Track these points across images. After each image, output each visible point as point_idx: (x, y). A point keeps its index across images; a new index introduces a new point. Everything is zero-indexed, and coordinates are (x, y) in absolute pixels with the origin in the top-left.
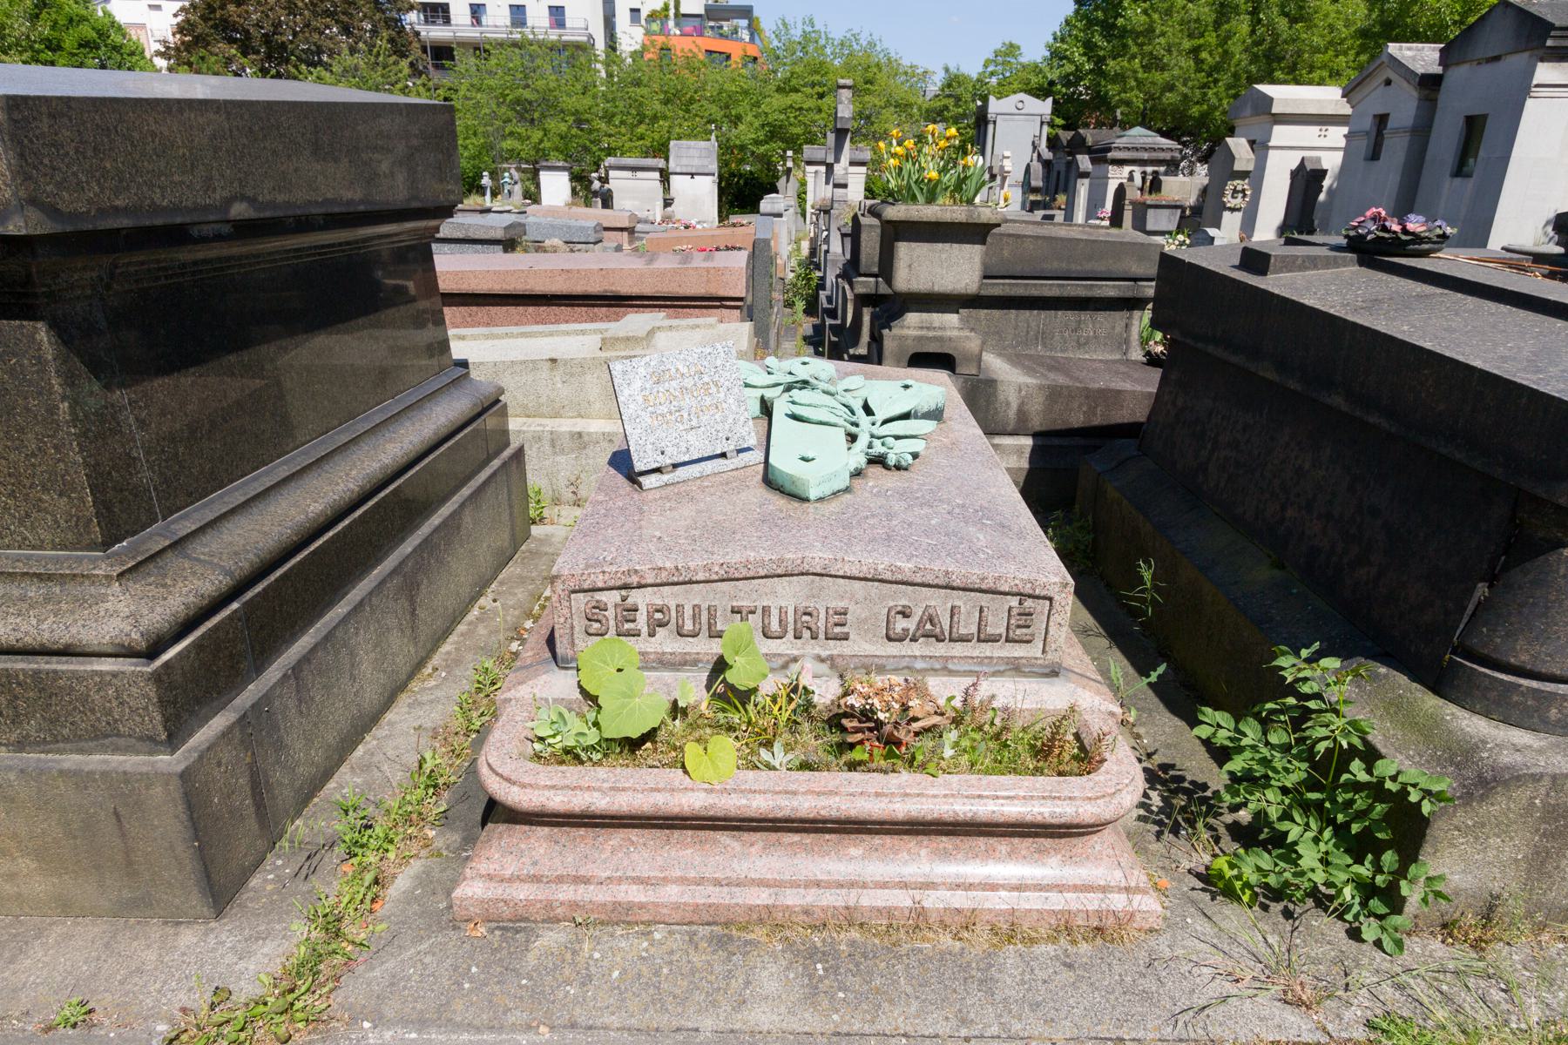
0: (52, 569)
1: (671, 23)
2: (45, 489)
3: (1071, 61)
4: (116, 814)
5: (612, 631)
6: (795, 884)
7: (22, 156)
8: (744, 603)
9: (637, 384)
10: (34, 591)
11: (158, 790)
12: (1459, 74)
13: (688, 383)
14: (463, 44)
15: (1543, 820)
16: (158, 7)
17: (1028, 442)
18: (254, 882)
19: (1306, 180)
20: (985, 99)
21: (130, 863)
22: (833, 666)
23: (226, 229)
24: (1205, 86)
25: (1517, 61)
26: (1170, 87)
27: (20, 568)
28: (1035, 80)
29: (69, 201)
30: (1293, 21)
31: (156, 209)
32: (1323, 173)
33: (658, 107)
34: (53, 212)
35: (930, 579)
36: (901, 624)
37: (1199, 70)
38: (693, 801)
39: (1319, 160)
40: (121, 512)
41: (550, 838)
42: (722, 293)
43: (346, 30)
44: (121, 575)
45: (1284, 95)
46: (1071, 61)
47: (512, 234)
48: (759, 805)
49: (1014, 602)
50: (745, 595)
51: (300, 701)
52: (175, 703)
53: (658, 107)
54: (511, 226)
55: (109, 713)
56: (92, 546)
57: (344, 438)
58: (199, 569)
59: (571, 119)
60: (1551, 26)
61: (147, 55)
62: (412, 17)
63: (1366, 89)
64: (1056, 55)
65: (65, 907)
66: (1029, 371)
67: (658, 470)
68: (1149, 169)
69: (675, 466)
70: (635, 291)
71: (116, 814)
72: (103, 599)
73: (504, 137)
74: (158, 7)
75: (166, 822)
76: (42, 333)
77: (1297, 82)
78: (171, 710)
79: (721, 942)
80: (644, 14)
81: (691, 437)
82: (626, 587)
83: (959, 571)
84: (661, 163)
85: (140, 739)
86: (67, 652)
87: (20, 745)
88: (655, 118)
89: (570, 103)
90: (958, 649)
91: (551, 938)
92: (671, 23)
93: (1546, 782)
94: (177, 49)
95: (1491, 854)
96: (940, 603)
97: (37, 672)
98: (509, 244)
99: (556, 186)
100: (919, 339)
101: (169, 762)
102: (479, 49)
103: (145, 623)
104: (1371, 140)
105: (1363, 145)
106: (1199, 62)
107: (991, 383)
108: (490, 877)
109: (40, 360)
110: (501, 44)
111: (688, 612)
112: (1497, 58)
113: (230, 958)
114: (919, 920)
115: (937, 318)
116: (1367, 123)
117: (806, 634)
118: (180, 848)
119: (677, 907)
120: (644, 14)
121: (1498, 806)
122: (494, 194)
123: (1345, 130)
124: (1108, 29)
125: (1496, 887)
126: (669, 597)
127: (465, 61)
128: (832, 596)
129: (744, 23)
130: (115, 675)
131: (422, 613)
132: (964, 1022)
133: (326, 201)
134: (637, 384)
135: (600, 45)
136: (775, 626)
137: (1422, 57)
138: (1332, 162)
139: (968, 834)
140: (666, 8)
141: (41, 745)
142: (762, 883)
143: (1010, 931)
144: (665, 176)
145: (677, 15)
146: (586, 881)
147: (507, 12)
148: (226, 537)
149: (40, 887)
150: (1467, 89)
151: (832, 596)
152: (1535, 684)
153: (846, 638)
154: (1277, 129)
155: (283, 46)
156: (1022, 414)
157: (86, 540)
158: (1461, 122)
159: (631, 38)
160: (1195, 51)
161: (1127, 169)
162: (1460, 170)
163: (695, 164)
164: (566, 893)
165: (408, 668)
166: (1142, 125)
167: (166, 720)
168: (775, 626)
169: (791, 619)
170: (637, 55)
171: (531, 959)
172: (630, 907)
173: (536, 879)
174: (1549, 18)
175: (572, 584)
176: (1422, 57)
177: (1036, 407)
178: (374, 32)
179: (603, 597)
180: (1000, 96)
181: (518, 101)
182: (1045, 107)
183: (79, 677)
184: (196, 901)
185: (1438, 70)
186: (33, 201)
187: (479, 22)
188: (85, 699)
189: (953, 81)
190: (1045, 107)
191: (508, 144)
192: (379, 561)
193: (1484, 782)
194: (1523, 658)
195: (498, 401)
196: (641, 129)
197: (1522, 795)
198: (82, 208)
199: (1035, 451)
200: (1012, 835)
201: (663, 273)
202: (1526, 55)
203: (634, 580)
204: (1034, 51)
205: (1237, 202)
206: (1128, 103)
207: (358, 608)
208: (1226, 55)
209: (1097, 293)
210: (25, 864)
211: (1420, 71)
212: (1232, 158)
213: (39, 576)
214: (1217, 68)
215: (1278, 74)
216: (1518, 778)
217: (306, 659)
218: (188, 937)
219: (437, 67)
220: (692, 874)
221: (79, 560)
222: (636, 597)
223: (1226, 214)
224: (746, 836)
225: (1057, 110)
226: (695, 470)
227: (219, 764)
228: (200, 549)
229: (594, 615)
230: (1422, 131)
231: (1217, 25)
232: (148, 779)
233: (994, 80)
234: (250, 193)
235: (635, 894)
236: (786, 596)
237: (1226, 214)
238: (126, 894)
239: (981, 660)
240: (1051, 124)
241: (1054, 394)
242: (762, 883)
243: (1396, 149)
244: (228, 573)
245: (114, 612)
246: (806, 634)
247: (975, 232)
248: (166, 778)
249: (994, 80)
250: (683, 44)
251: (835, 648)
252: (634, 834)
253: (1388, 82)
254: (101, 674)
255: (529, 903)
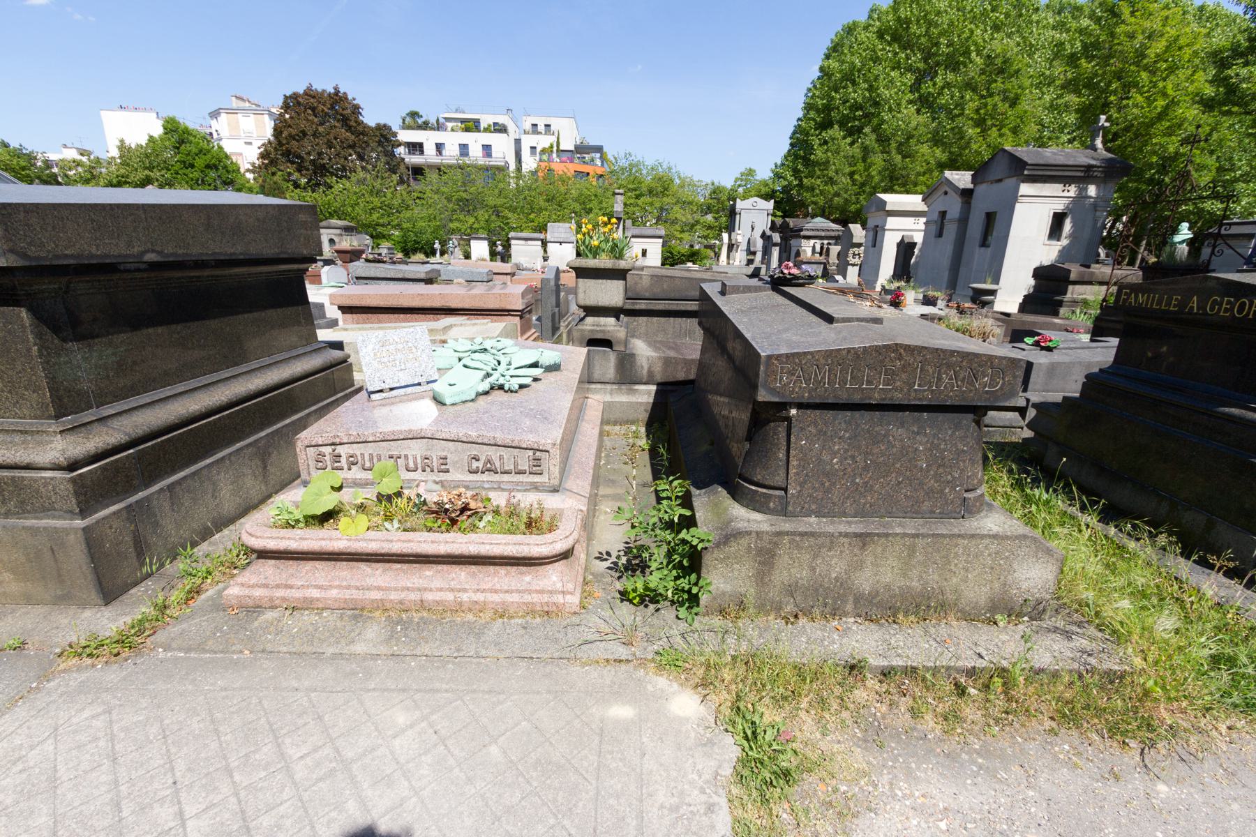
0: (28, 428)
1: (554, 155)
2: (26, 389)
3: (785, 179)
4: (52, 549)
5: (329, 467)
6: (396, 589)
7: (6, 230)
8: (395, 453)
9: (370, 347)
10: (18, 438)
11: (72, 537)
12: (982, 189)
13: (400, 346)
14: (431, 166)
15: (757, 555)
16: (250, 143)
17: (654, 388)
18: (132, 591)
19: (906, 248)
20: (734, 200)
21: (60, 576)
22: (443, 486)
23: (143, 266)
24: (859, 194)
25: (1010, 182)
26: (837, 194)
27: (12, 427)
28: (764, 190)
29: (33, 251)
30: (904, 157)
31: (93, 256)
32: (915, 244)
33: (542, 203)
34: (24, 256)
35: (485, 441)
36: (475, 464)
37: (854, 184)
38: (339, 545)
39: (912, 237)
40: (66, 404)
41: (275, 566)
42: (509, 307)
43: (361, 158)
44: (61, 432)
45: (893, 200)
46: (785, 179)
47: (430, 276)
48: (373, 547)
49: (531, 453)
50: (395, 449)
51: (173, 504)
52: (85, 494)
53: (542, 203)
54: (433, 271)
55: (50, 498)
56: (50, 417)
57: (227, 375)
58: (111, 432)
59: (491, 211)
60: (1026, 163)
61: (242, 170)
62: (401, 151)
63: (935, 196)
64: (778, 176)
65: (29, 600)
66: (656, 349)
67: (381, 391)
68: (826, 242)
69: (391, 389)
70: (460, 306)
71: (52, 549)
72: (51, 442)
73: (451, 221)
74: (250, 143)
75: (77, 555)
76: (24, 313)
77: (908, 192)
78: (82, 498)
79: (355, 617)
80: (538, 150)
81: (401, 374)
82: (333, 444)
83: (500, 437)
84: (542, 236)
85: (66, 512)
86: (28, 467)
87: (7, 515)
88: (541, 210)
89: (491, 201)
90: (506, 478)
91: (270, 615)
92: (554, 155)
93: (754, 535)
94: (260, 167)
95: (736, 573)
96: (493, 453)
97: (13, 477)
98: (429, 281)
99: (480, 248)
100: (592, 331)
101: (79, 523)
102: (439, 169)
103: (68, 454)
104: (938, 226)
105: (934, 228)
106: (854, 182)
107: (633, 355)
108: (243, 585)
109: (23, 326)
110: (450, 167)
111: (367, 458)
112: (1000, 180)
113: (106, 621)
114: (458, 608)
115: (603, 320)
116: (935, 216)
117: (428, 469)
118: (84, 568)
119: (336, 600)
120: (538, 150)
121: (733, 547)
122: (442, 254)
123: (924, 220)
124: (807, 162)
125: (743, 590)
126: (356, 450)
127: (433, 176)
128: (438, 450)
129: (598, 155)
130: (52, 479)
131: (272, 469)
132: (458, 650)
133: (214, 253)
134: (370, 347)
135: (512, 167)
136: (411, 465)
137: (962, 179)
138: (918, 238)
139: (484, 564)
140: (552, 147)
141: (17, 515)
142: (379, 588)
143: (501, 613)
144: (544, 243)
145: (558, 150)
146: (291, 587)
147: (457, 148)
148: (134, 419)
149: (14, 587)
150: (986, 197)
151: (438, 450)
152: (764, 491)
153: (448, 471)
154: (889, 219)
155: (323, 166)
156: (650, 372)
157: (46, 414)
158: (983, 216)
159: (529, 163)
160: (852, 174)
161: (812, 242)
162: (984, 243)
163: (562, 237)
164: (280, 593)
165: (260, 497)
166: (823, 216)
167: (79, 503)
168: (411, 465)
169: (419, 461)
170: (534, 173)
171: (256, 624)
172: (312, 600)
173: (266, 586)
174: (1025, 159)
175: (306, 443)
176: (962, 179)
177: (658, 369)
178: (378, 159)
179: (323, 449)
180: (744, 198)
181: (460, 200)
182: (770, 205)
183: (34, 480)
184: (94, 596)
185: (971, 186)
186: (12, 251)
187: (441, 154)
188: (37, 491)
189: (716, 191)
190: (770, 205)
191: (452, 225)
192: (240, 439)
193: (729, 536)
194: (758, 478)
195: (346, 361)
196: (532, 216)
197: (744, 541)
198: (43, 254)
199: (657, 392)
200: (506, 564)
201: (475, 296)
202: (1014, 179)
203: (337, 441)
204: (764, 173)
205: (857, 260)
206: (815, 203)
207: (217, 461)
208: (870, 176)
209: (637, 307)
210: (7, 576)
211: (962, 187)
212: (852, 236)
213: (21, 431)
214: (863, 185)
215: (896, 187)
216: (740, 533)
217: (179, 482)
218: (88, 613)
219: (415, 179)
220: (345, 583)
221: (42, 424)
222: (340, 449)
223: (850, 268)
224: (374, 565)
225: (778, 206)
226: (402, 391)
227: (111, 527)
228: (115, 423)
229: (320, 458)
230: (964, 220)
231: (864, 160)
232: (66, 531)
233: (741, 190)
234: (159, 249)
235: (315, 593)
236: (415, 450)
237: (850, 268)
238: (59, 592)
239: (518, 483)
240: (774, 215)
241: (667, 362)
242: (379, 588)
243: (951, 230)
244: (129, 435)
245: (56, 447)
246: (428, 469)
247: (620, 274)
248: (75, 530)
249: (741, 190)
250: (558, 166)
251: (443, 477)
252: (317, 564)
253: (946, 193)
254: (45, 478)
255: (261, 598)
